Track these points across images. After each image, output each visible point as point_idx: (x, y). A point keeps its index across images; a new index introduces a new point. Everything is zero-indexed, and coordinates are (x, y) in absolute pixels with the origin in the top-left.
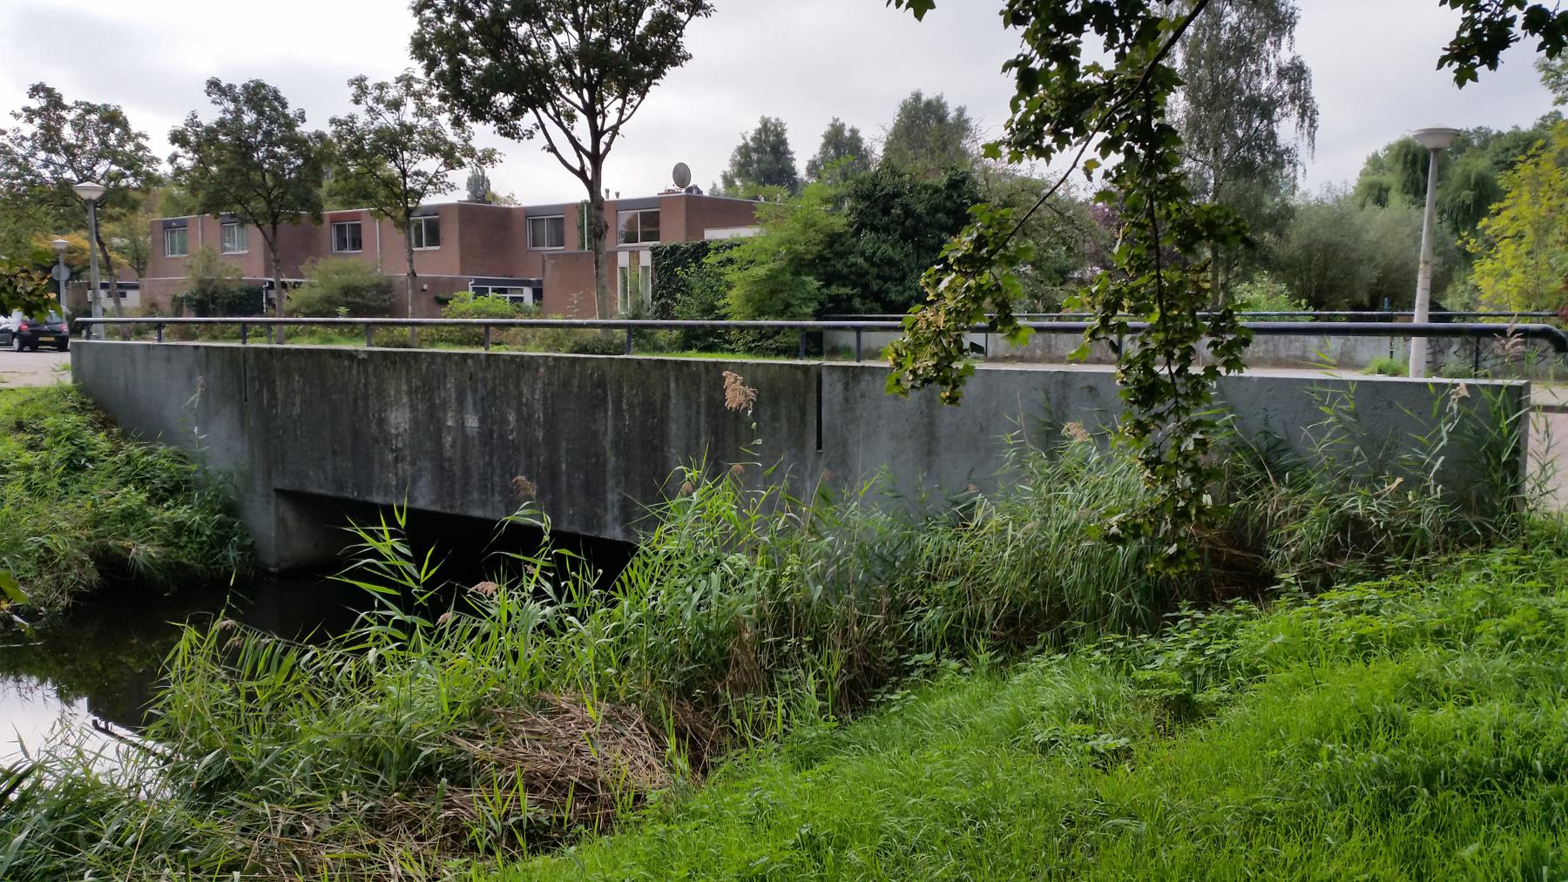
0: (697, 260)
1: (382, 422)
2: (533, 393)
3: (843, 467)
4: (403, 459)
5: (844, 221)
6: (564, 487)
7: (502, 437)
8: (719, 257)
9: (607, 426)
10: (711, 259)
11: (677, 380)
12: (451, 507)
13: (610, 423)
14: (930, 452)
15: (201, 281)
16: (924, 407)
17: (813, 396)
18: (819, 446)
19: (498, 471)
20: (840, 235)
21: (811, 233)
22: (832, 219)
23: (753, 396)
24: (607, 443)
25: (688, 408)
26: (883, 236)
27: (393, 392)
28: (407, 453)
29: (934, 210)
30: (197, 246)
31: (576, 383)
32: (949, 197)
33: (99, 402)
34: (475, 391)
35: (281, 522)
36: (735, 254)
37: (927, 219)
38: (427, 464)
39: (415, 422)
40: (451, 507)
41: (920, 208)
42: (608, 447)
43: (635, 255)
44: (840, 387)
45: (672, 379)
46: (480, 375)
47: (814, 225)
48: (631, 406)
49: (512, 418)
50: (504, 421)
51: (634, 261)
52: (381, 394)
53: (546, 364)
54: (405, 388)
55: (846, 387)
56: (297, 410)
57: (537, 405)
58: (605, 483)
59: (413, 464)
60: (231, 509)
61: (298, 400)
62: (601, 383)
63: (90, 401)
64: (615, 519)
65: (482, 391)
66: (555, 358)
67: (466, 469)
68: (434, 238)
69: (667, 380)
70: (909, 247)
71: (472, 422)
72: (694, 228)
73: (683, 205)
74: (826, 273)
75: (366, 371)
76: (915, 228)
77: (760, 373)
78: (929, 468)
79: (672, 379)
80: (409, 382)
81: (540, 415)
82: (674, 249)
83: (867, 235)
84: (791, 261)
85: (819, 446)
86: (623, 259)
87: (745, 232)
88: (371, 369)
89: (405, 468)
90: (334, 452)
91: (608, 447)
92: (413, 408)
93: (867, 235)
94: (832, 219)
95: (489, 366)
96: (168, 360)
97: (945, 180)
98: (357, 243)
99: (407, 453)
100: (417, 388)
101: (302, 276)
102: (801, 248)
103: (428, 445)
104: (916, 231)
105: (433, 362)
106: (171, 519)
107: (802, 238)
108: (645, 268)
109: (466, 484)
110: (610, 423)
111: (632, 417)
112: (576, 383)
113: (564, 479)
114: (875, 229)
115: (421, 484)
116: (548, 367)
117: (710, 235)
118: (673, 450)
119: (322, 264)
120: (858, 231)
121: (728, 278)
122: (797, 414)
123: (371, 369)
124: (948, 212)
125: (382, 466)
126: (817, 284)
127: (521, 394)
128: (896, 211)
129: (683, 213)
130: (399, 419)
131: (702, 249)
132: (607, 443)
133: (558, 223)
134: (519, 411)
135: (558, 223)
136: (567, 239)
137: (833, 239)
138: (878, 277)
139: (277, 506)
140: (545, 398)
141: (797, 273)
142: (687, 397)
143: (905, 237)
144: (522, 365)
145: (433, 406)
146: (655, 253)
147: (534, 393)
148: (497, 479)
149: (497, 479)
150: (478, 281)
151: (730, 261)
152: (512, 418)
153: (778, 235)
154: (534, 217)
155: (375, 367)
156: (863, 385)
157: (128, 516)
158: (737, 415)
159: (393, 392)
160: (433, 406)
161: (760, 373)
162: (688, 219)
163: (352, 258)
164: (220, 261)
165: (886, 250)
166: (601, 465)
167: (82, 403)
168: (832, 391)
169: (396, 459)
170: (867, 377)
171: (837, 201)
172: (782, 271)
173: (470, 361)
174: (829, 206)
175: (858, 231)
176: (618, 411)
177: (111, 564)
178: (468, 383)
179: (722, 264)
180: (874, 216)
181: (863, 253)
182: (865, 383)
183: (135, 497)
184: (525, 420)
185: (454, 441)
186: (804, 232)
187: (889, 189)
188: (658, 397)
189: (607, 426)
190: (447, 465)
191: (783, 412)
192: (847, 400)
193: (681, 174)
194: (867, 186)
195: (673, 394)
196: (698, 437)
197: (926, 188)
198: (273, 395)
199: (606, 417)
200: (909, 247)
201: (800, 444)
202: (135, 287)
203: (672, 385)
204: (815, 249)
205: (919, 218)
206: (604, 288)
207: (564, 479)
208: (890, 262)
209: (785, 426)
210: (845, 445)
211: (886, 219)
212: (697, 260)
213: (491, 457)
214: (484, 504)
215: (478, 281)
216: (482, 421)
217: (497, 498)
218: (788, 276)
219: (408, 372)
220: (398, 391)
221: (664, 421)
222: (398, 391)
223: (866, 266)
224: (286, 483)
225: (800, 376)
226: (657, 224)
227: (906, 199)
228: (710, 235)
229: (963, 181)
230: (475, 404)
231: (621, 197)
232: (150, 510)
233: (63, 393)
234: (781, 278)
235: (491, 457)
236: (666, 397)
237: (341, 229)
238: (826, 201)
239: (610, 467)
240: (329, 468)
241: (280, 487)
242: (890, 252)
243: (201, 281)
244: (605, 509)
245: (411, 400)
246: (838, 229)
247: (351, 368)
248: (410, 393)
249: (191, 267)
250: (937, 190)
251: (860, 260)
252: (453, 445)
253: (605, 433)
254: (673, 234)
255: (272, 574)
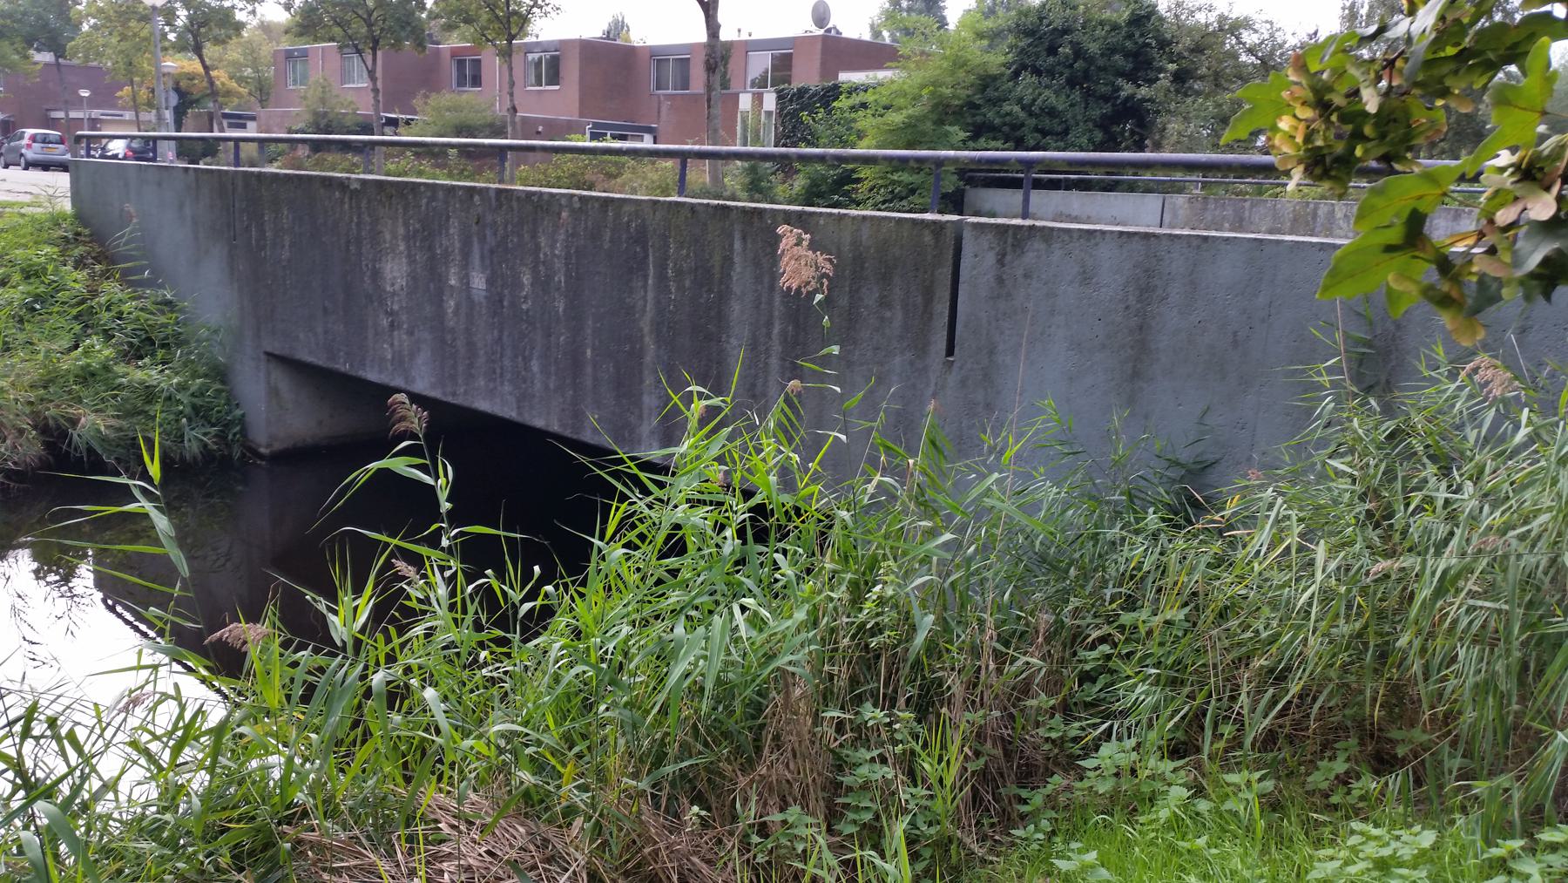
0: (826, 105)
1: (376, 275)
2: (553, 247)
3: (981, 405)
4: (399, 327)
5: (1002, 59)
6: (589, 382)
7: (513, 305)
8: (850, 102)
9: (646, 300)
10: (843, 103)
11: (744, 238)
12: (454, 394)
13: (650, 295)
14: (1136, 375)
15: (316, 114)
16: (1132, 300)
17: (945, 273)
18: (950, 351)
19: (508, 352)
20: (995, 78)
21: (961, 74)
22: (987, 57)
23: (828, 269)
24: (645, 324)
25: (758, 279)
26: (1045, 81)
27: (388, 237)
28: (404, 318)
29: (1110, 50)
30: (316, 75)
31: (607, 235)
32: (1130, 36)
33: (90, 236)
34: (483, 239)
35: (274, 392)
36: (869, 97)
37: (1101, 62)
38: (426, 336)
39: (413, 277)
40: (454, 394)
41: (1093, 48)
42: (646, 330)
43: (758, 99)
44: (991, 259)
45: (737, 236)
46: (489, 218)
47: (965, 64)
48: (679, 273)
49: (526, 279)
50: (517, 284)
51: (757, 106)
52: (375, 236)
53: (570, 205)
54: (401, 231)
55: (1001, 262)
56: (286, 254)
57: (558, 265)
58: (641, 381)
59: (410, 333)
60: (220, 374)
61: (287, 240)
62: (641, 237)
63: (87, 232)
64: (652, 433)
65: (491, 241)
66: (581, 198)
67: (470, 345)
68: (554, 78)
69: (731, 236)
70: (1077, 95)
71: (479, 282)
72: (829, 69)
73: (819, 46)
74: (974, 124)
75: (359, 208)
76: (1086, 72)
77: (866, 232)
78: (1131, 401)
79: (737, 236)
80: (406, 225)
81: (560, 278)
82: (802, 92)
83: (1027, 79)
84: (935, 106)
85: (950, 351)
86: (745, 102)
87: (881, 75)
88: (364, 204)
89: (401, 337)
90: (325, 310)
91: (646, 330)
92: (411, 260)
93: (1027, 79)
94: (987, 57)
95: (500, 206)
96: (159, 184)
97: (1126, 15)
98: (476, 81)
99: (404, 318)
100: (416, 231)
101: (415, 113)
102: (948, 92)
103: (428, 310)
104: (1086, 76)
105: (433, 198)
106: (142, 383)
107: (949, 79)
108: (769, 114)
109: (471, 366)
110: (650, 295)
111: (680, 288)
112: (607, 235)
113: (589, 370)
114: (1037, 72)
115: (420, 362)
116: (573, 211)
117: (847, 77)
118: (734, 341)
119: (434, 100)
120: (1016, 74)
121: (859, 125)
122: (919, 299)
123: (364, 204)
124: (1127, 55)
125: (376, 334)
126: (963, 135)
127: (538, 248)
128: (1066, 50)
129: (818, 56)
130: (395, 272)
131: (834, 92)
132: (645, 324)
133: (684, 64)
134: (535, 271)
135: (684, 64)
136: (692, 84)
137: (987, 82)
138: (1036, 130)
139: (269, 374)
140: (568, 257)
141: (940, 122)
142: (757, 263)
143: (1072, 83)
144: (540, 206)
145: (433, 258)
146: (781, 97)
147: (553, 245)
148: (507, 362)
149: (507, 362)
150: (596, 125)
151: (864, 105)
152: (526, 279)
153: (919, 77)
154: (658, 57)
155: (369, 202)
156: (1029, 258)
157: (87, 376)
158: (797, 302)
159: (388, 237)
160: (433, 258)
161: (866, 232)
162: (823, 64)
163: (470, 94)
164: (335, 92)
165: (1049, 97)
166: (637, 355)
167: (78, 234)
168: (978, 263)
169: (392, 325)
170: (1038, 244)
171: (994, 36)
172: (921, 119)
173: (477, 198)
174: (985, 42)
175: (1016, 74)
176: (662, 277)
177: (55, 436)
178: (475, 228)
179: (853, 108)
180: (1038, 56)
181: (1020, 101)
182: (1033, 252)
183: (101, 351)
184: (543, 284)
185: (458, 306)
186: (953, 73)
187: (1058, 24)
188: (717, 259)
189: (646, 300)
190: (449, 337)
191: (897, 293)
192: (1000, 280)
193: (821, 17)
194: (1033, 19)
195: (737, 259)
196: (769, 324)
197: (1102, 23)
198: (262, 232)
199: (645, 286)
200: (1077, 95)
201: (920, 348)
202: (253, 118)
203: (737, 245)
204: (963, 93)
205: (1090, 60)
206: (716, 131)
207: (589, 370)
208: (1052, 112)
209: (899, 315)
210: (991, 353)
211: (1051, 59)
212: (826, 105)
213: (501, 332)
214: (491, 393)
215: (596, 125)
216: (490, 282)
217: (507, 388)
218: (929, 126)
219: (406, 209)
220: (395, 237)
221: (723, 297)
222: (395, 237)
223: (1022, 115)
224: (276, 347)
225: (928, 238)
226: (789, 67)
227: (1076, 37)
228: (847, 77)
229: (1148, 17)
230: (482, 258)
231: (754, 37)
232: (120, 369)
233: (56, 220)
234: (921, 127)
235: (501, 332)
236: (728, 261)
237: (461, 64)
238: (980, 35)
239: (648, 359)
240: (320, 330)
241: (269, 349)
242: (1053, 99)
243: (316, 114)
244: (641, 417)
245: (408, 248)
246: (994, 71)
247: (342, 202)
248: (407, 238)
249: (305, 98)
250: (1115, 27)
251: (1017, 109)
252: (456, 312)
253: (644, 311)
254: (807, 76)
255: (261, 457)
